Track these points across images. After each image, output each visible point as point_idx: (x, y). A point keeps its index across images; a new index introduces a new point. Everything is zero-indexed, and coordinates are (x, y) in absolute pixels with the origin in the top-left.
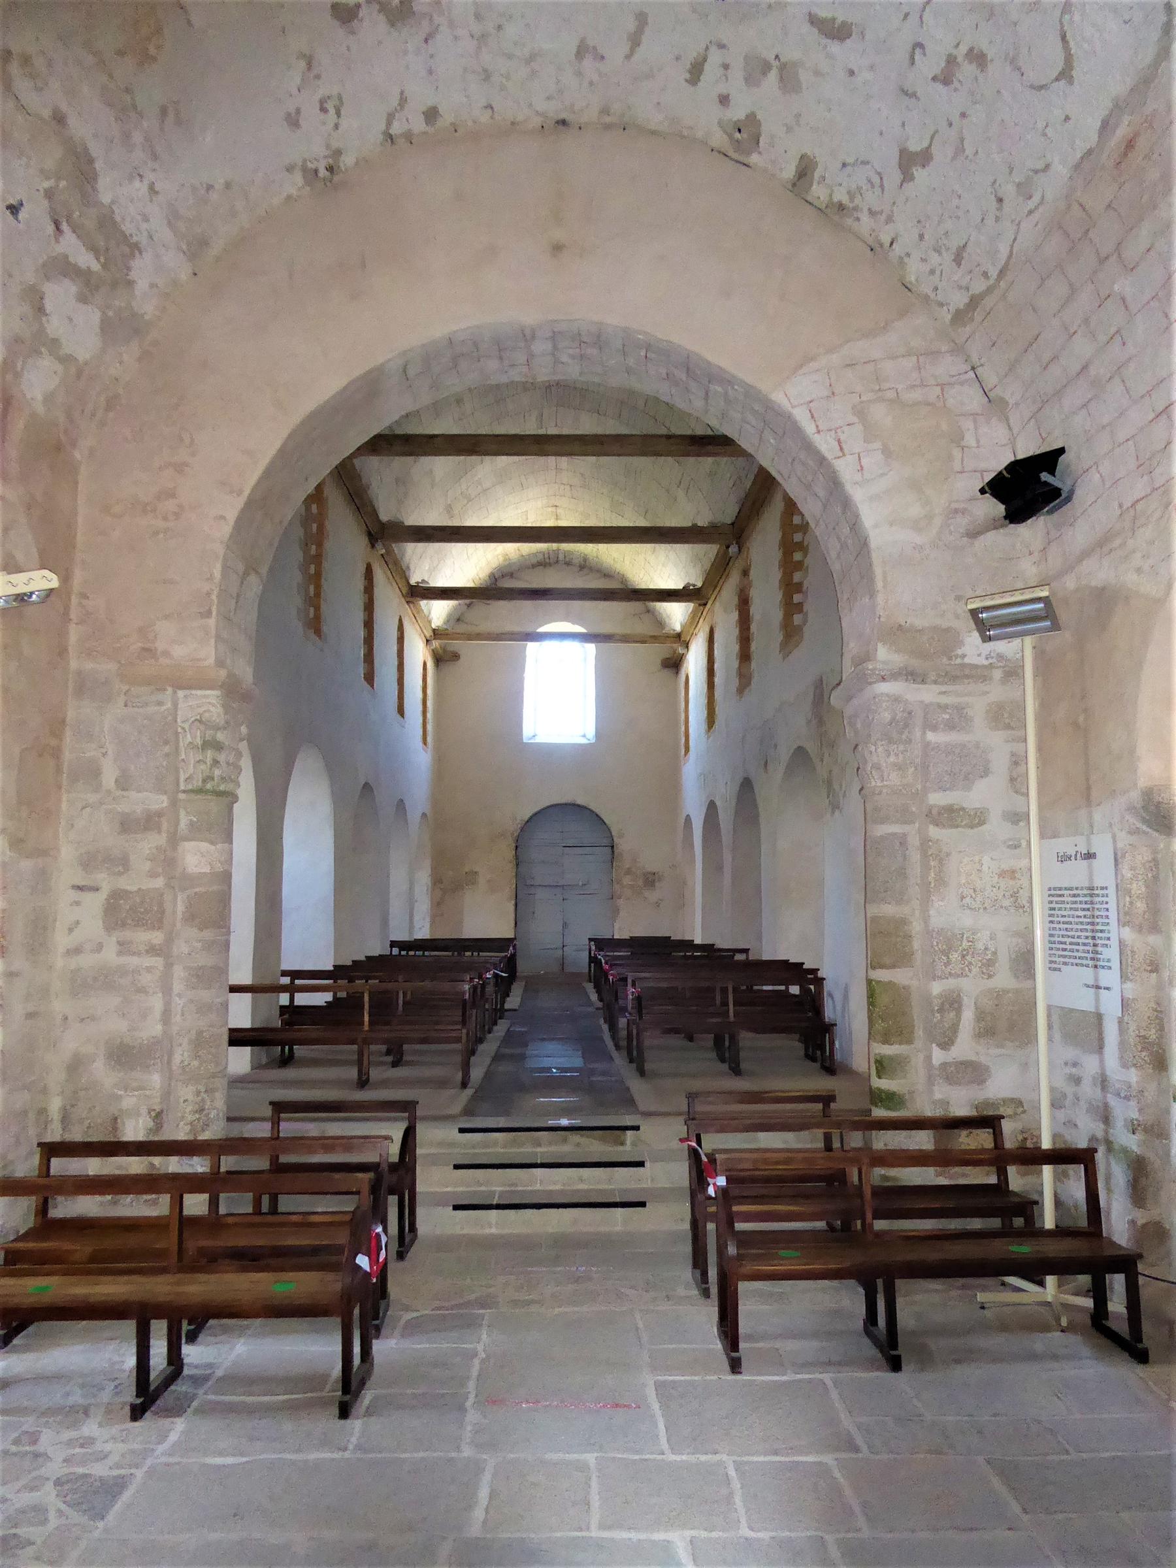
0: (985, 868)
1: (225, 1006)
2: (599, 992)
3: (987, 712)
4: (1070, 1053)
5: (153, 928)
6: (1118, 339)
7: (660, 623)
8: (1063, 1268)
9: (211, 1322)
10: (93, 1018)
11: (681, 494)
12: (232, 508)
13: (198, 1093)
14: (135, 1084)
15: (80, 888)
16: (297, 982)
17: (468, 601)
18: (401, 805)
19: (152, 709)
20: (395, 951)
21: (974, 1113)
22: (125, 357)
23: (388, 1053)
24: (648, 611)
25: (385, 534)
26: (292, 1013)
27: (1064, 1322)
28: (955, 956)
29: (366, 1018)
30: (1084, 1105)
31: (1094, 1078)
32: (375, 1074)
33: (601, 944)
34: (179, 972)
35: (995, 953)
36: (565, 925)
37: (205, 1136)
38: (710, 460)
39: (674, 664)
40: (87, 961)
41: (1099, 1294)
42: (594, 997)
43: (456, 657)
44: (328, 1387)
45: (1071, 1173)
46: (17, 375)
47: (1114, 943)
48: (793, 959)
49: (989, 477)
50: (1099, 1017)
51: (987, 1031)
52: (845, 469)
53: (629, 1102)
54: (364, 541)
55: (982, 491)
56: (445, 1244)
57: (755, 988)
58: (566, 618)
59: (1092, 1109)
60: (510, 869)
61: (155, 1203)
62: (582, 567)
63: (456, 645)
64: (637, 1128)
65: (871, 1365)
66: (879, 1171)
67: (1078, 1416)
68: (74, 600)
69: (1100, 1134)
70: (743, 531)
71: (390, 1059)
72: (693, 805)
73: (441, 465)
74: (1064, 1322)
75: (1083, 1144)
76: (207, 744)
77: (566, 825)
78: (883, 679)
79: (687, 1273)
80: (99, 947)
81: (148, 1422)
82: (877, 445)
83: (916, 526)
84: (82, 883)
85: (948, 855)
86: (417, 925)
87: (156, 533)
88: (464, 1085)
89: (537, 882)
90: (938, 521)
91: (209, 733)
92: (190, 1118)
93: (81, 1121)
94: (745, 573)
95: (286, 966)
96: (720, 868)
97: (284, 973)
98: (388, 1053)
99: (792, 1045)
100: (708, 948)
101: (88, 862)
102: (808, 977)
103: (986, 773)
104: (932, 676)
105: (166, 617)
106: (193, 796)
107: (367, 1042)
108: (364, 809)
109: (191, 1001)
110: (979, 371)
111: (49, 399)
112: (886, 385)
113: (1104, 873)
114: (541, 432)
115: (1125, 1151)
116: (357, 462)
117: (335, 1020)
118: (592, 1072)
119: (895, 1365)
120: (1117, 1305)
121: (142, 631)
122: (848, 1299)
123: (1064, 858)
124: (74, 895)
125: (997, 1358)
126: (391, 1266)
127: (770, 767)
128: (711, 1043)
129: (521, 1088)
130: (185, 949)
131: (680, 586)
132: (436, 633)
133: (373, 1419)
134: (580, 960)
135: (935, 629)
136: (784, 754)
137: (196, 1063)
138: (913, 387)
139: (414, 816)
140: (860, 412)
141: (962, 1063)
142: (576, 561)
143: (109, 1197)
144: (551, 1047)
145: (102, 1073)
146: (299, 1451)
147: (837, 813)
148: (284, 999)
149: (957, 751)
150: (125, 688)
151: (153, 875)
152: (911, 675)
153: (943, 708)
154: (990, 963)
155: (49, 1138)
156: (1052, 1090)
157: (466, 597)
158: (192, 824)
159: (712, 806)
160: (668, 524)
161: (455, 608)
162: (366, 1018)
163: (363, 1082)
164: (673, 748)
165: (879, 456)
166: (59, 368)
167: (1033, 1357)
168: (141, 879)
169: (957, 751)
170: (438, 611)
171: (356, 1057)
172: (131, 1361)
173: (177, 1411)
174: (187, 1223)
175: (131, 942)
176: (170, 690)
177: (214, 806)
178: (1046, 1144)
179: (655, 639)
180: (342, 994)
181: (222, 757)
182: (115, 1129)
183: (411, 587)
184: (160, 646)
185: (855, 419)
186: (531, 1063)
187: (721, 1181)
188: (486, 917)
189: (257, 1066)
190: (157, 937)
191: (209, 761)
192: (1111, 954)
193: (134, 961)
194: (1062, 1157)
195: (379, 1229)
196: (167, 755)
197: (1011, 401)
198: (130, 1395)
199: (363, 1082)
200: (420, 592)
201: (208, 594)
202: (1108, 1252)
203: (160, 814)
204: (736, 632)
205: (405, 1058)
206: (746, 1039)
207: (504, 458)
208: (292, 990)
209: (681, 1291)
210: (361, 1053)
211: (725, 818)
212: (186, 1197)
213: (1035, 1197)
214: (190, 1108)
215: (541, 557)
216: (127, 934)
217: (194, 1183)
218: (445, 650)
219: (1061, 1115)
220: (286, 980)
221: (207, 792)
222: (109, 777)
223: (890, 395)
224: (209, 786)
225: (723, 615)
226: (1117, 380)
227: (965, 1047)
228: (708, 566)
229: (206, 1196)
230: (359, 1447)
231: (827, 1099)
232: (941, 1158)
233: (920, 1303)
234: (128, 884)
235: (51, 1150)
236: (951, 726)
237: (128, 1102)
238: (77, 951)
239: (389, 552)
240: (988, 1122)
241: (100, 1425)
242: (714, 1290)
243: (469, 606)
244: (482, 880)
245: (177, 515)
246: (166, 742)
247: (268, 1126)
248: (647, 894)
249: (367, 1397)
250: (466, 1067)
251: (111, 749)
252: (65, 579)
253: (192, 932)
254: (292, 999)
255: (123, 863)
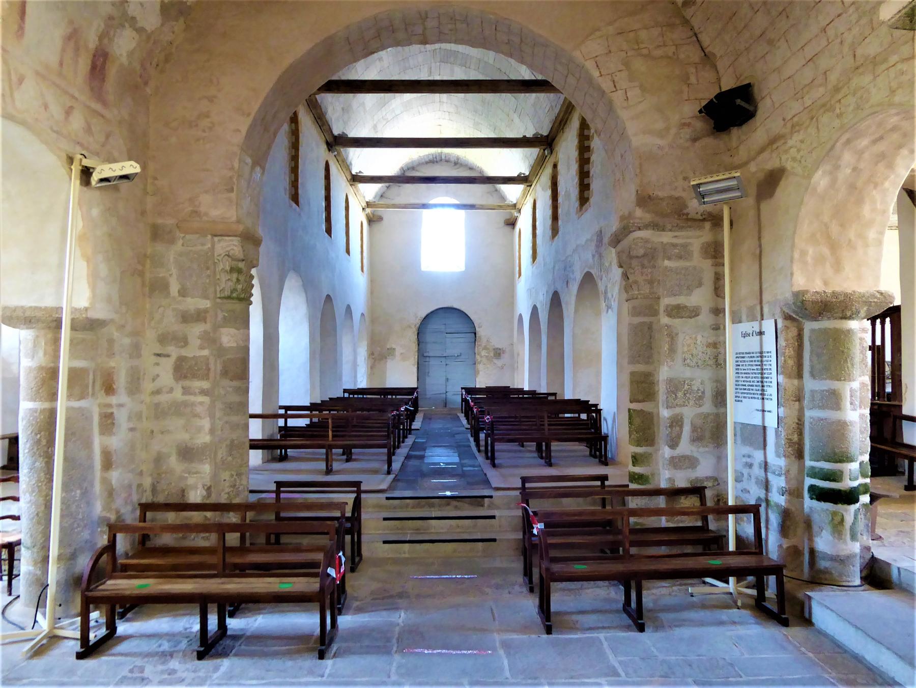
0: (698, 342)
1: (247, 427)
2: (468, 419)
3: (701, 248)
4: (746, 450)
5: (203, 379)
6: (784, 13)
7: (503, 198)
8: (740, 573)
9: (243, 605)
10: (168, 432)
11: (516, 117)
12: (244, 125)
13: (232, 476)
14: (194, 470)
15: (159, 355)
16: (289, 412)
17: (387, 184)
18: (349, 308)
19: (200, 248)
20: (346, 395)
21: (688, 485)
22: (176, 29)
23: (343, 454)
24: (496, 190)
25: (338, 142)
26: (286, 431)
27: (739, 604)
28: (680, 394)
29: (330, 433)
30: (753, 480)
31: (760, 464)
32: (336, 466)
33: (469, 391)
34: (219, 405)
35: (703, 393)
36: (447, 380)
37: (237, 501)
38: (534, 95)
39: (512, 223)
40: (163, 398)
41: (760, 587)
42: (465, 422)
43: (380, 219)
44: (313, 641)
45: (745, 519)
46: (111, 40)
47: (775, 384)
48: (583, 398)
49: (704, 103)
50: (764, 428)
51: (697, 438)
52: (617, 98)
53: (486, 482)
54: (324, 147)
55: (700, 112)
56: (379, 562)
57: (561, 415)
58: (447, 194)
59: (758, 482)
60: (414, 347)
61: (208, 539)
62: (456, 164)
63: (380, 211)
64: (491, 497)
65: (628, 628)
66: (632, 520)
67: (746, 656)
68: (150, 181)
69: (763, 496)
70: (553, 140)
71: (345, 457)
72: (523, 308)
73: (369, 99)
74: (739, 604)
75: (753, 502)
76: (232, 270)
77: (446, 324)
78: (640, 229)
79: (520, 579)
80: (171, 390)
81: (206, 664)
82: (636, 84)
83: (661, 134)
84: (159, 352)
85: (677, 334)
86: (359, 380)
87: (198, 140)
88: (389, 473)
89: (431, 354)
90: (673, 131)
91: (234, 262)
92: (227, 490)
93: (163, 491)
94: (555, 166)
95: (282, 403)
96: (539, 346)
97: (281, 407)
98: (343, 454)
99: (581, 448)
100: (533, 393)
101: (163, 339)
102: (592, 409)
103: (700, 285)
104: (669, 226)
105: (206, 192)
106: (225, 301)
107: (330, 448)
108: (327, 318)
109: (227, 422)
110: (699, 36)
111: (131, 54)
112: (642, 46)
113: (769, 344)
114: (431, 78)
115: (777, 505)
116: (319, 97)
117: (311, 436)
118: (463, 465)
119: (641, 628)
120: (771, 592)
121: (191, 200)
122: (614, 594)
123: (745, 335)
124: (155, 359)
125: (702, 624)
126: (349, 576)
127: (570, 285)
128: (534, 449)
129: (424, 475)
130: (222, 392)
131: (515, 174)
132: (369, 204)
133: (338, 659)
134: (456, 399)
135: (671, 197)
136: (578, 276)
137: (230, 458)
138: (659, 46)
139: (356, 316)
140: (627, 64)
141: (682, 457)
142: (452, 159)
143: (181, 535)
144: (439, 451)
145: (174, 462)
146: (295, 677)
147: (610, 311)
148: (281, 422)
149: (683, 272)
150: (182, 235)
151: (202, 348)
152: (655, 226)
153: (674, 246)
154: (701, 398)
155: (143, 501)
156: (736, 471)
157: (385, 182)
158: (225, 317)
159: (535, 310)
160: (508, 136)
161: (380, 189)
162: (330, 433)
163: (329, 471)
164: (511, 275)
165: (637, 91)
166: (136, 36)
167: (721, 623)
168: (195, 350)
169: (683, 272)
170: (370, 191)
171: (325, 457)
172: (197, 627)
173: (224, 654)
174: (227, 550)
175: (190, 387)
176: (209, 237)
177: (237, 306)
178: (731, 502)
179: (500, 207)
180: (315, 420)
181: (242, 278)
182: (183, 496)
183: (353, 176)
184: (203, 209)
185: (624, 68)
186: (426, 461)
187: (541, 526)
188: (401, 375)
189: (266, 461)
190: (205, 385)
191: (234, 280)
192: (772, 391)
193: (192, 398)
194: (740, 510)
195: (341, 554)
196: (209, 276)
197: (718, 56)
198: (196, 646)
199: (329, 471)
200: (356, 179)
201: (231, 178)
202: (766, 563)
203: (206, 311)
204: (550, 202)
205: (353, 457)
206: (555, 446)
207: (408, 94)
208: (286, 417)
209: (517, 588)
210: (327, 454)
211: (543, 316)
212: (227, 535)
213: (724, 533)
214: (227, 484)
215: (431, 157)
216: (187, 383)
217: (233, 528)
218: (373, 215)
219: (739, 486)
220: (282, 412)
221: (233, 299)
222: (174, 288)
223: (645, 52)
224: (234, 295)
225: (541, 192)
226: (783, 40)
227: (685, 447)
228: (532, 162)
229: (238, 534)
230: (330, 675)
231: (603, 478)
232: (669, 512)
233: (657, 594)
234: (188, 352)
235: (145, 508)
236: (680, 257)
237: (191, 481)
238: (158, 392)
239: (339, 153)
240: (697, 491)
241: (180, 663)
242: (537, 590)
243: (388, 187)
244: (397, 353)
245: (211, 129)
246: (208, 268)
247: (274, 495)
248: (495, 361)
249: (335, 647)
250: (390, 465)
251: (174, 271)
252: (144, 167)
253: (226, 382)
254: (286, 422)
255: (184, 342)
